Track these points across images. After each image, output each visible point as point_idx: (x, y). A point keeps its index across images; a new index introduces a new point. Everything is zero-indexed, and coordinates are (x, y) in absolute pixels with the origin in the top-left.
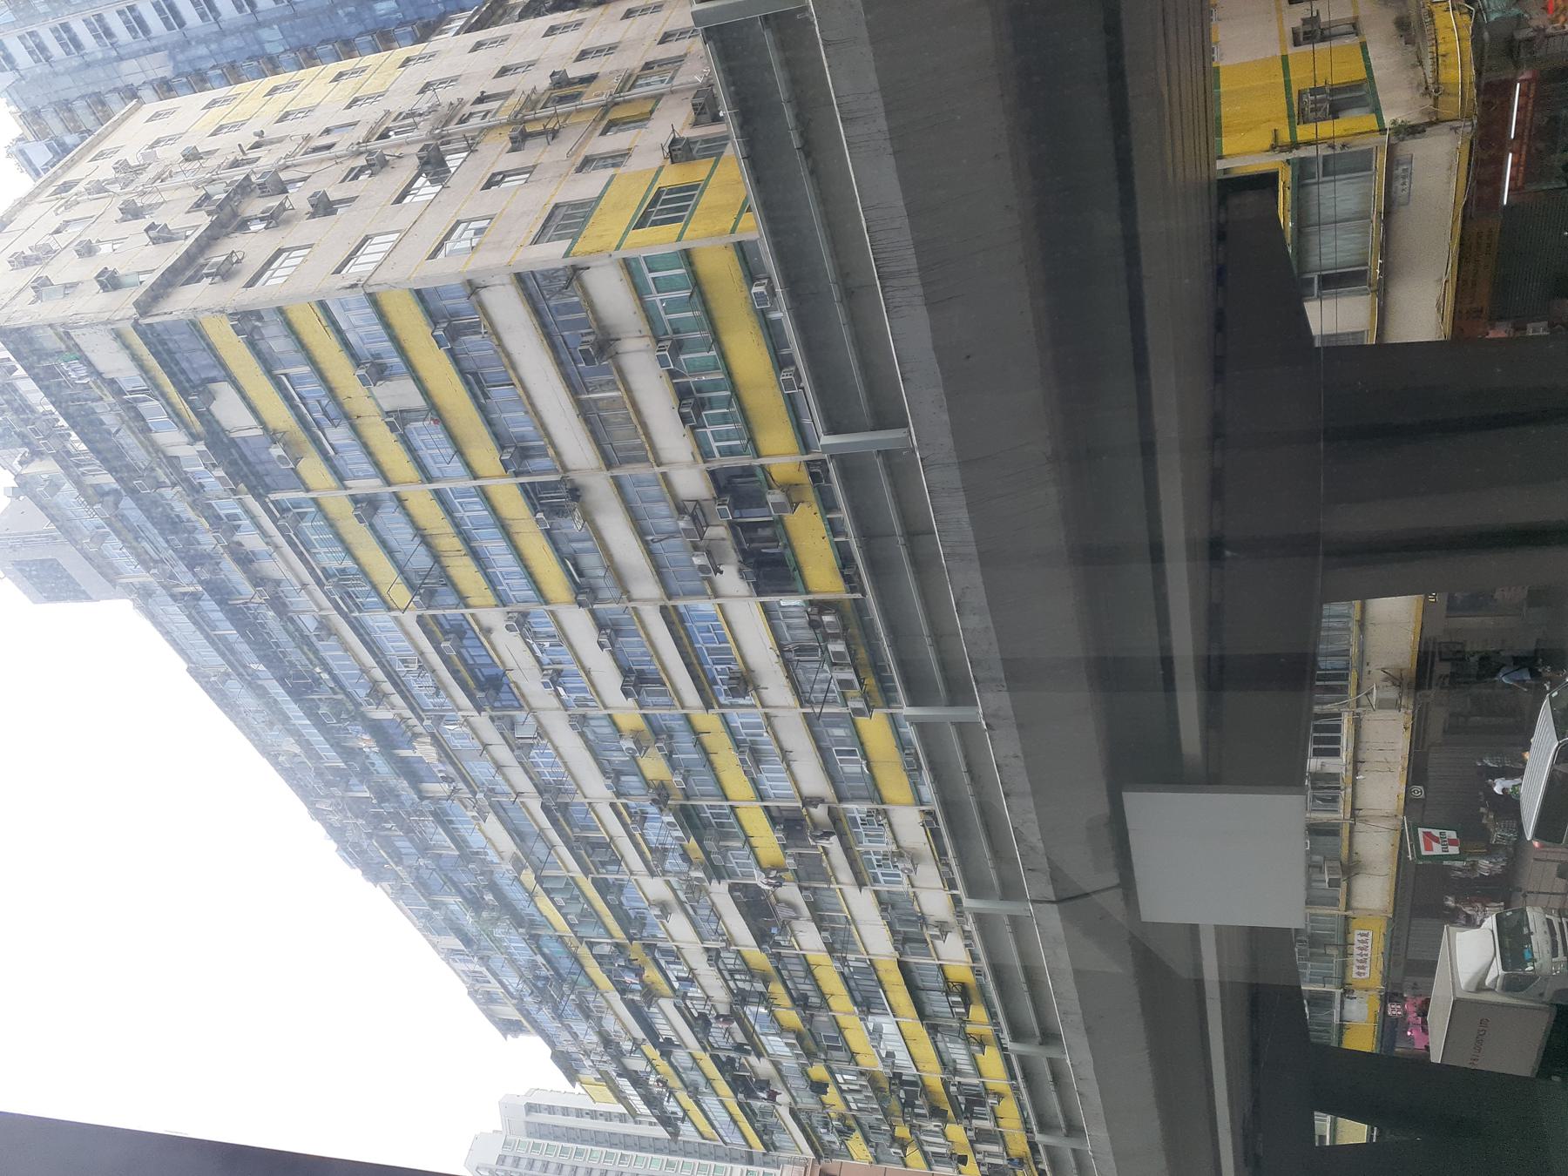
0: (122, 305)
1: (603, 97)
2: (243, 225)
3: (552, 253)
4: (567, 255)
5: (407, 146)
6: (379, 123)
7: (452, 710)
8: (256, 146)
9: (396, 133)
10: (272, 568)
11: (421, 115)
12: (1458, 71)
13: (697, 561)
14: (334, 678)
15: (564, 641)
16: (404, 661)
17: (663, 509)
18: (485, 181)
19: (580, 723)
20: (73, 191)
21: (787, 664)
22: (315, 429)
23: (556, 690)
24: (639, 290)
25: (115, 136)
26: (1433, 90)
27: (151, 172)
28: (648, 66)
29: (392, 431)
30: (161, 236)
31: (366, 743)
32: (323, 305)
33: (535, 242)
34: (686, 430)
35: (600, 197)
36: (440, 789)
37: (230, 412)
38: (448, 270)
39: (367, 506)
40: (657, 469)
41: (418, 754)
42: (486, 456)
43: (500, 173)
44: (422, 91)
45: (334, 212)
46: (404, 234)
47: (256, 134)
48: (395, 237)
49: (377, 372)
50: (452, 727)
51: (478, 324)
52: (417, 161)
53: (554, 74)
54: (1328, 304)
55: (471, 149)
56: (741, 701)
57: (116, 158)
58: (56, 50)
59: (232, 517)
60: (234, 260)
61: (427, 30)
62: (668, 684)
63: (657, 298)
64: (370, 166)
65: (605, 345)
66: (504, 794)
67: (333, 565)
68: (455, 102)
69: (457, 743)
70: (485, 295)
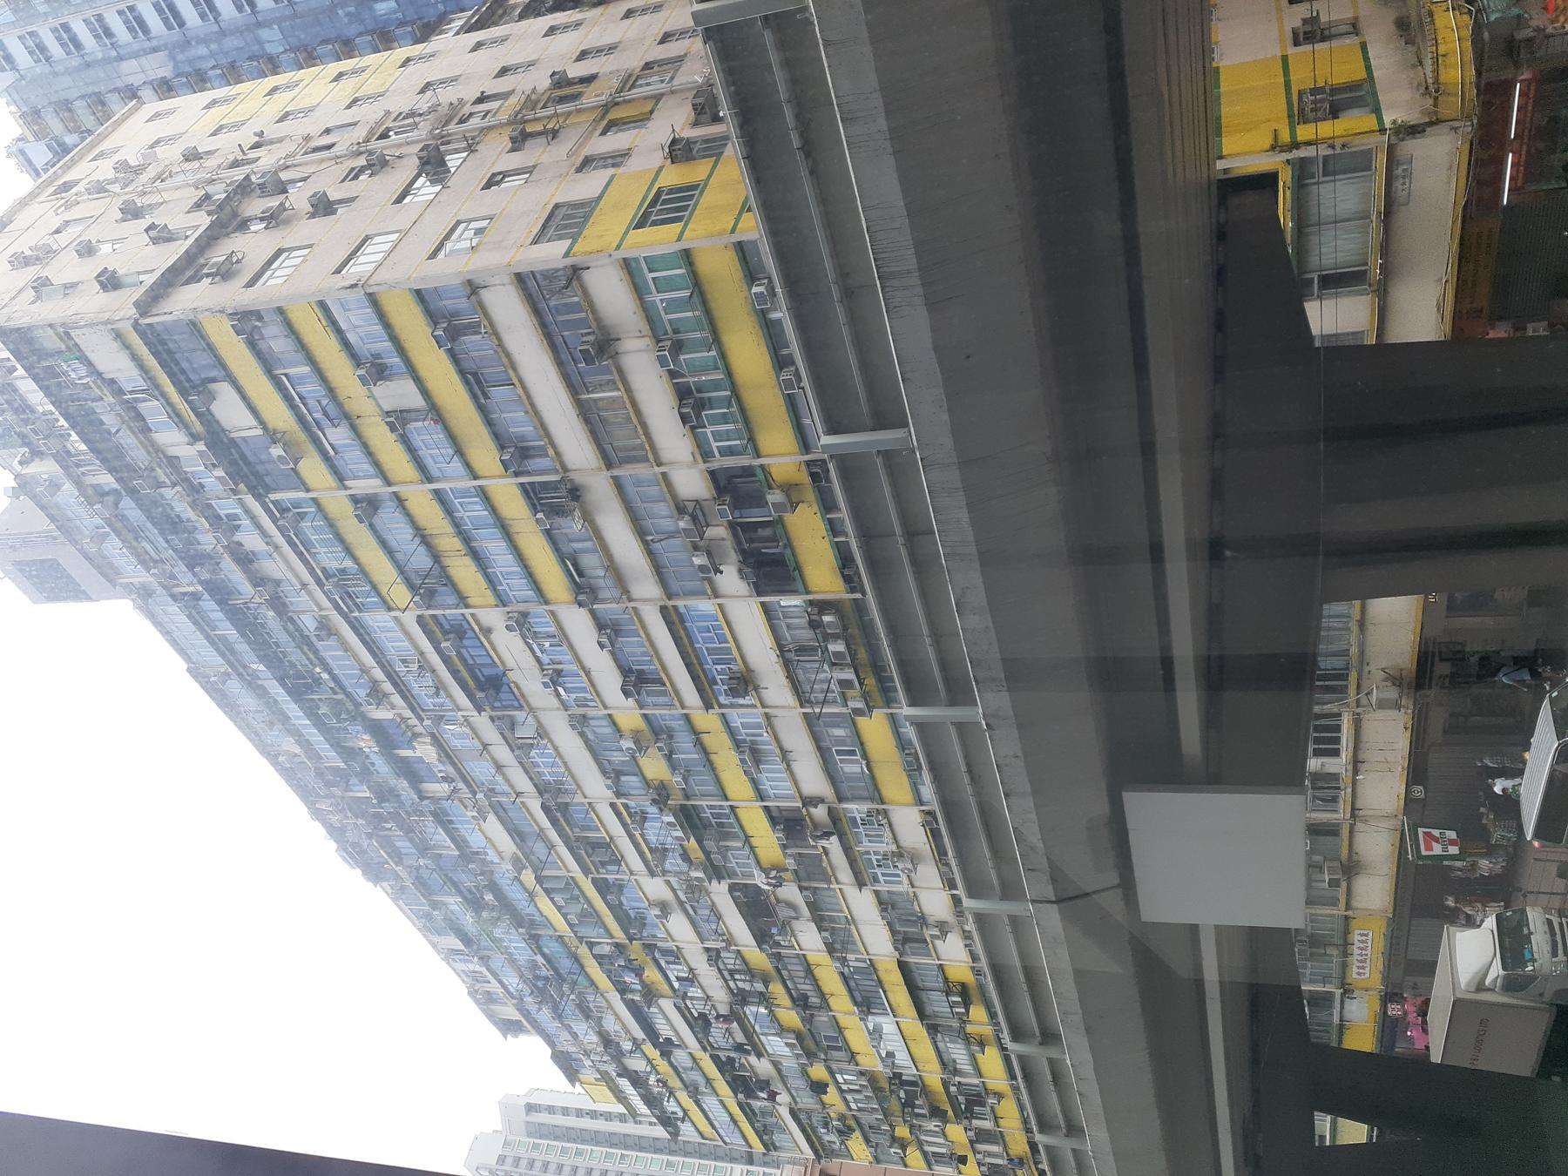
0: (122, 305)
1: (603, 97)
2: (243, 225)
3: (552, 253)
4: (567, 255)
5: (407, 146)
6: (379, 123)
7: (452, 710)
8: (256, 146)
9: (396, 133)
10: (272, 568)
11: (421, 115)
12: (1458, 71)
13: (697, 561)
14: (334, 678)
15: (564, 641)
16: (404, 661)
17: (663, 509)
18: (485, 181)
19: (580, 723)
20: (73, 191)
21: (787, 664)
22: (315, 429)
23: (556, 690)
24: (639, 290)
25: (115, 136)
26: (1433, 90)
27: (151, 172)
28: (648, 66)
29: (392, 431)
30: (161, 236)
31: (366, 743)
32: (323, 305)
33: (535, 242)
34: (686, 430)
35: (600, 197)
36: (440, 789)
37: (230, 412)
38: (448, 270)
39: (367, 506)
40: (657, 469)
41: (418, 754)
42: (486, 456)
43: (500, 173)
44: (422, 91)
45: (334, 212)
46: (404, 234)
47: (256, 134)
48: (395, 237)
49: (377, 372)
50: (452, 727)
51: (478, 324)
52: (417, 161)
53: (554, 74)
54: (1328, 304)
55: (471, 149)
56: (741, 701)
57: (116, 158)
58: (56, 50)
59: (232, 517)
60: (234, 260)
61: (427, 30)
62: (668, 684)
63: (657, 298)
64: (370, 166)
65: (605, 345)
66: (504, 794)
67: (333, 565)
68: (455, 102)
69: (457, 743)
70: (485, 295)
